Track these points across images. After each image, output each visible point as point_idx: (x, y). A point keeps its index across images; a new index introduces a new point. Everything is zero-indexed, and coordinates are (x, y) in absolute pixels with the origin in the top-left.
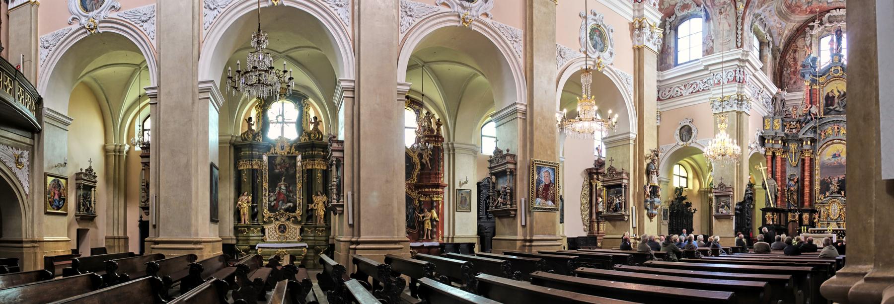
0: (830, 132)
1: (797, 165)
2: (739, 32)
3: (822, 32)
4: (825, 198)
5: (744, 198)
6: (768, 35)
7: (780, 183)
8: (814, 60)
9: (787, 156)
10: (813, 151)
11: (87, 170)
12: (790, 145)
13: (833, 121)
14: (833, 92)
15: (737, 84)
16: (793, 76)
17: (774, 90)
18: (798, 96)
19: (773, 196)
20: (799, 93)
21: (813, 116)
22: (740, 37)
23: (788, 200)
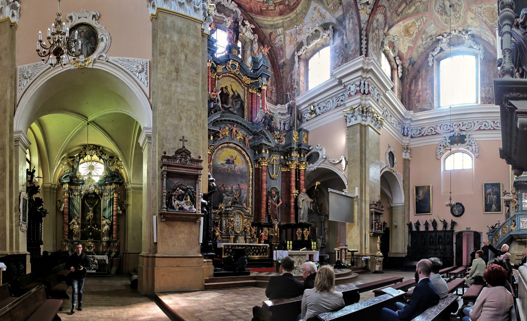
4: (226, 207)
11: (377, 202)
14: (227, 89)
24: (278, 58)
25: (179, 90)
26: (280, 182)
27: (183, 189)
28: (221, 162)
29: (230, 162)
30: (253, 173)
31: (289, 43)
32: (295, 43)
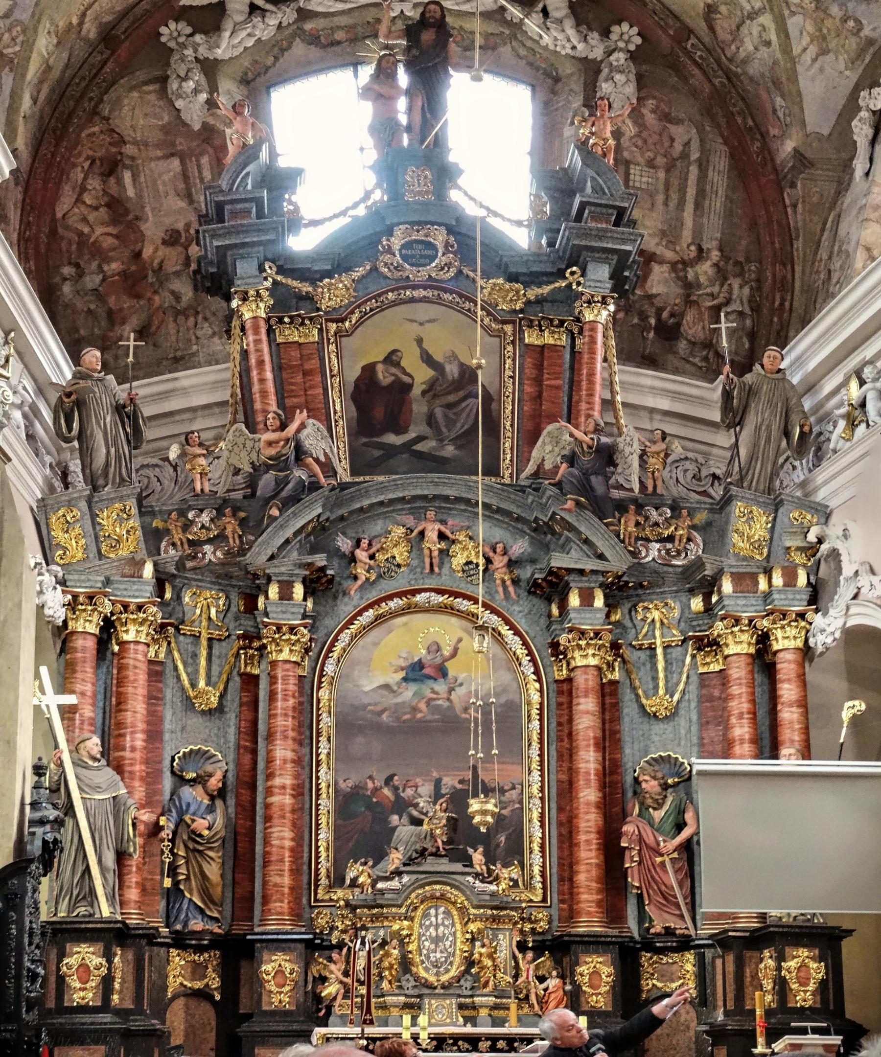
0: (400, 553)
1: (220, 709)
5: (20, 844)
7: (140, 792)
9: (169, 652)
12: (187, 599)
13: (415, 498)
14: (397, 365)
16: (127, 303)
18: (185, 391)
19: (110, 859)
20: (186, 378)
23: (176, 883)
24: (773, 131)
26: (694, 729)
28: (380, 681)
29: (427, 671)
30: (541, 704)
31: (813, 50)
32: (852, 43)
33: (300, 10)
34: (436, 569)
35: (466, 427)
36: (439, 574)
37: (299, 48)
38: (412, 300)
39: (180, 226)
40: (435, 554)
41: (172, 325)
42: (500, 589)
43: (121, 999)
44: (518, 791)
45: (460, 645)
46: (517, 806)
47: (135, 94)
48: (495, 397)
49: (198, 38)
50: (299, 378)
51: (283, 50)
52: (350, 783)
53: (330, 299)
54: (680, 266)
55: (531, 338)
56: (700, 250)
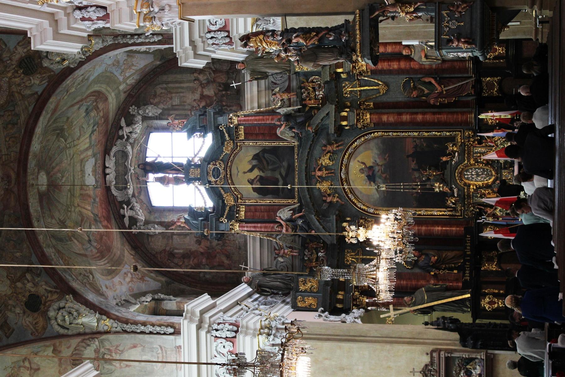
2: (150, 329)
3: (141, 202)
6: (143, 299)
8: (193, 213)
10: (362, 219)
14: (253, 180)
15: (240, 337)
17: (243, 289)
21: (297, 215)
22: (158, 329)
25: (360, 368)
27: (460, 371)
31: (133, 68)
33: (132, 197)
34: (333, 171)
35: (275, 157)
36: (334, 170)
37: (142, 197)
38: (231, 175)
39: (195, 239)
40: (327, 172)
41: (227, 248)
42: (340, 148)
43: (502, 290)
44: (416, 140)
45: (360, 161)
46: (422, 140)
47: (151, 244)
48: (263, 148)
49: (138, 224)
50: (258, 214)
51: (142, 202)
52: (415, 202)
53: (231, 201)
54: (203, 86)
55: (242, 137)
56: (195, 80)
